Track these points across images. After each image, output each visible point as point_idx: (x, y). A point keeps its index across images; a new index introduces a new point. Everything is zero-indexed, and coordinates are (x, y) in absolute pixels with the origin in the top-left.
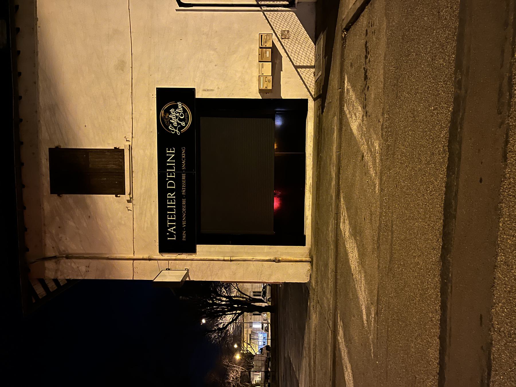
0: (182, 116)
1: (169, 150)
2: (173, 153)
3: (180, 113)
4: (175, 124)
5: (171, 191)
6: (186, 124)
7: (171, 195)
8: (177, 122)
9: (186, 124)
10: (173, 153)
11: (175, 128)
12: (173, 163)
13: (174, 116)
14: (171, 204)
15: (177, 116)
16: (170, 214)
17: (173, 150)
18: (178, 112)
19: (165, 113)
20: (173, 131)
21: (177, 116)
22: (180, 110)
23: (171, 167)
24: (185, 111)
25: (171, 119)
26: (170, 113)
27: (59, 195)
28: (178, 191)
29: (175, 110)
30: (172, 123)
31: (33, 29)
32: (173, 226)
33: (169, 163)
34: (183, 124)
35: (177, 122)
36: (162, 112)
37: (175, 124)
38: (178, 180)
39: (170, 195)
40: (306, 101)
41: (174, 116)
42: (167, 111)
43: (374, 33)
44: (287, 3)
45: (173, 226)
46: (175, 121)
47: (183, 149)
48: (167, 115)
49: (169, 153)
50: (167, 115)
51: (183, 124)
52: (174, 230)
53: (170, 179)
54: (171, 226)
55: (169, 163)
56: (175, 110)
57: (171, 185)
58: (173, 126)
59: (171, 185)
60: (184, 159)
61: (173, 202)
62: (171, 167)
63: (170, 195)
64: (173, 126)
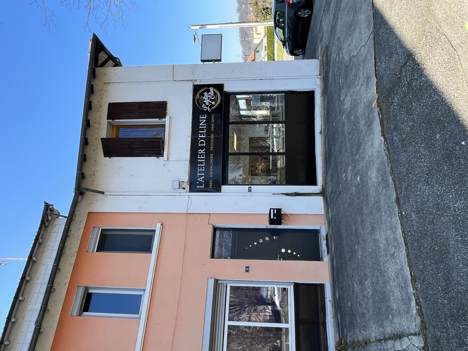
0: (213, 97)
1: (202, 117)
2: (204, 119)
4: (207, 104)
5: (202, 148)
6: (216, 103)
7: (202, 151)
10: (204, 119)
11: (207, 106)
12: (204, 126)
13: (206, 98)
14: (202, 125)
15: (209, 98)
16: (201, 133)
17: (204, 116)
19: (200, 96)
20: (205, 109)
21: (209, 98)
22: (212, 93)
23: (203, 129)
24: (215, 93)
25: (204, 99)
26: (204, 96)
28: (207, 148)
30: (205, 103)
32: (202, 176)
34: (213, 103)
36: (198, 95)
37: (207, 104)
38: (207, 140)
39: (200, 152)
40: (322, 286)
41: (206, 98)
42: (202, 94)
43: (394, 280)
45: (202, 176)
46: (207, 102)
49: (201, 119)
50: (202, 97)
51: (213, 103)
53: (201, 138)
54: (200, 176)
57: (202, 143)
59: (202, 143)
62: (203, 129)
63: (200, 152)
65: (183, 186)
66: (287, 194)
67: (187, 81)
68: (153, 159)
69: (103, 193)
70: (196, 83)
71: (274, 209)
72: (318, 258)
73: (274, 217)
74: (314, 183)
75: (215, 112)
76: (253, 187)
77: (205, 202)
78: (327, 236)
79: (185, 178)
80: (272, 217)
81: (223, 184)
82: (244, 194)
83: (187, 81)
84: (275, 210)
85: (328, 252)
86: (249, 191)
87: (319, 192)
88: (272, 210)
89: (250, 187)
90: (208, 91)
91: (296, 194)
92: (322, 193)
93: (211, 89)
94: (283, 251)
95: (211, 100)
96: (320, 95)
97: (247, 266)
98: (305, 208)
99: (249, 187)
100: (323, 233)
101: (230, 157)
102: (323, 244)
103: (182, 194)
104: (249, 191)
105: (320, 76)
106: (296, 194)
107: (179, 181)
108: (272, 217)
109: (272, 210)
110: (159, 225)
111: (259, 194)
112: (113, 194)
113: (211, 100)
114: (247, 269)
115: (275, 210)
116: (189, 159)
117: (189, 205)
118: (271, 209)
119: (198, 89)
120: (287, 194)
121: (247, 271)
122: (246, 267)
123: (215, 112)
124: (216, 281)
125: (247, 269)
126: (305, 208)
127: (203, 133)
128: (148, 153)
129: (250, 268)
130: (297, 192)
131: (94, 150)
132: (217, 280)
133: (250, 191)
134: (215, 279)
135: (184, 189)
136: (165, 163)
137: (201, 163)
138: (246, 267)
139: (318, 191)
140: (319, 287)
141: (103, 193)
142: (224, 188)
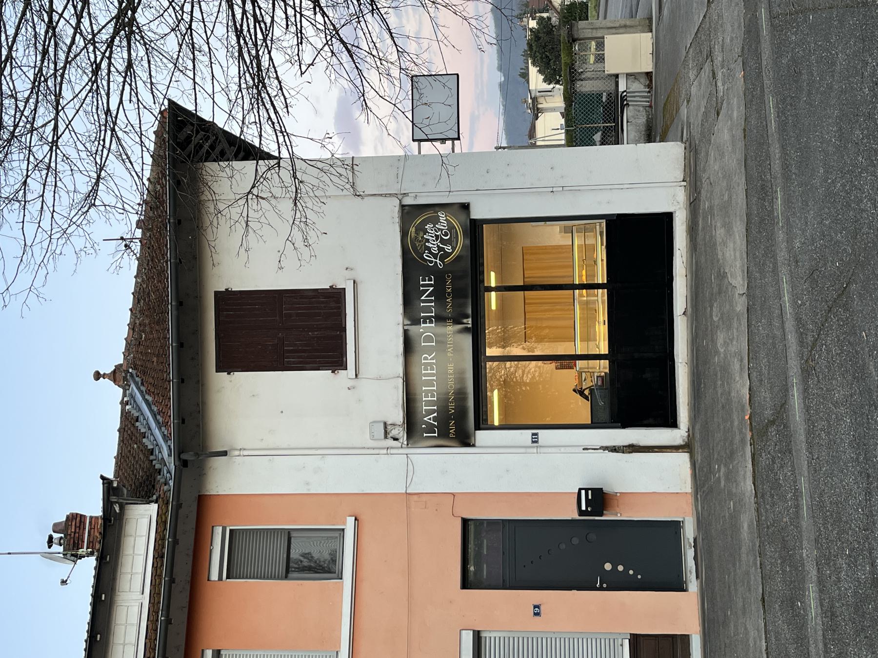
2: (430, 285)
3: (442, 230)
4: (435, 250)
6: (454, 249)
8: (438, 246)
9: (454, 249)
10: (430, 285)
12: (431, 301)
15: (437, 237)
16: (427, 392)
17: (430, 280)
18: (439, 229)
20: (431, 262)
21: (437, 237)
24: (451, 228)
25: (428, 241)
26: (425, 232)
27: (229, 374)
29: (434, 226)
30: (429, 249)
31: (195, 258)
33: (424, 301)
34: (448, 249)
35: (438, 246)
37: (435, 250)
39: (426, 358)
42: (421, 229)
44: (590, 497)
47: (449, 276)
48: (421, 234)
49: (423, 286)
50: (421, 234)
52: (435, 419)
55: (424, 301)
56: (434, 226)
58: (430, 253)
60: (449, 295)
61: (432, 369)
64: (430, 253)
65: (395, 432)
66: (614, 449)
67: (386, 195)
68: (324, 375)
69: (224, 453)
70: (408, 201)
71: (587, 490)
72: (679, 586)
73: (587, 507)
74: (673, 423)
75: (454, 269)
76: (541, 432)
77: (442, 470)
78: (695, 540)
79: (398, 416)
80: (584, 508)
81: (478, 427)
82: (523, 450)
83: (386, 195)
84: (590, 492)
85: (697, 577)
86: (533, 442)
87: (682, 443)
88: (583, 492)
89: (536, 434)
90: (436, 221)
91: (633, 449)
92: (686, 447)
93: (442, 216)
94: (608, 566)
95: (443, 242)
96: (686, 407)
97: (537, 617)
98: (652, 475)
99: (533, 434)
100: (689, 532)
101: (489, 364)
102: (690, 554)
103: (393, 451)
104: (533, 442)
105: (684, 183)
106: (633, 449)
107: (385, 424)
108: (584, 508)
109: (583, 492)
110: (351, 521)
111: (553, 450)
112: (246, 453)
113: (443, 242)
114: (537, 611)
115: (590, 492)
116: (401, 375)
117: (410, 474)
118: (580, 490)
119: (413, 215)
120: (614, 449)
121: (537, 614)
122: (535, 607)
123: (454, 269)
124: (478, 637)
125: (537, 611)
126: (652, 475)
127: (430, 318)
128: (315, 362)
129: (542, 608)
130: (635, 442)
131: (192, 359)
132: (479, 632)
133: (537, 442)
134: (474, 631)
135: (396, 439)
136: (351, 383)
137: (429, 403)
138: (535, 607)
139: (679, 442)
140: (679, 641)
141: (224, 453)
142: (482, 437)
